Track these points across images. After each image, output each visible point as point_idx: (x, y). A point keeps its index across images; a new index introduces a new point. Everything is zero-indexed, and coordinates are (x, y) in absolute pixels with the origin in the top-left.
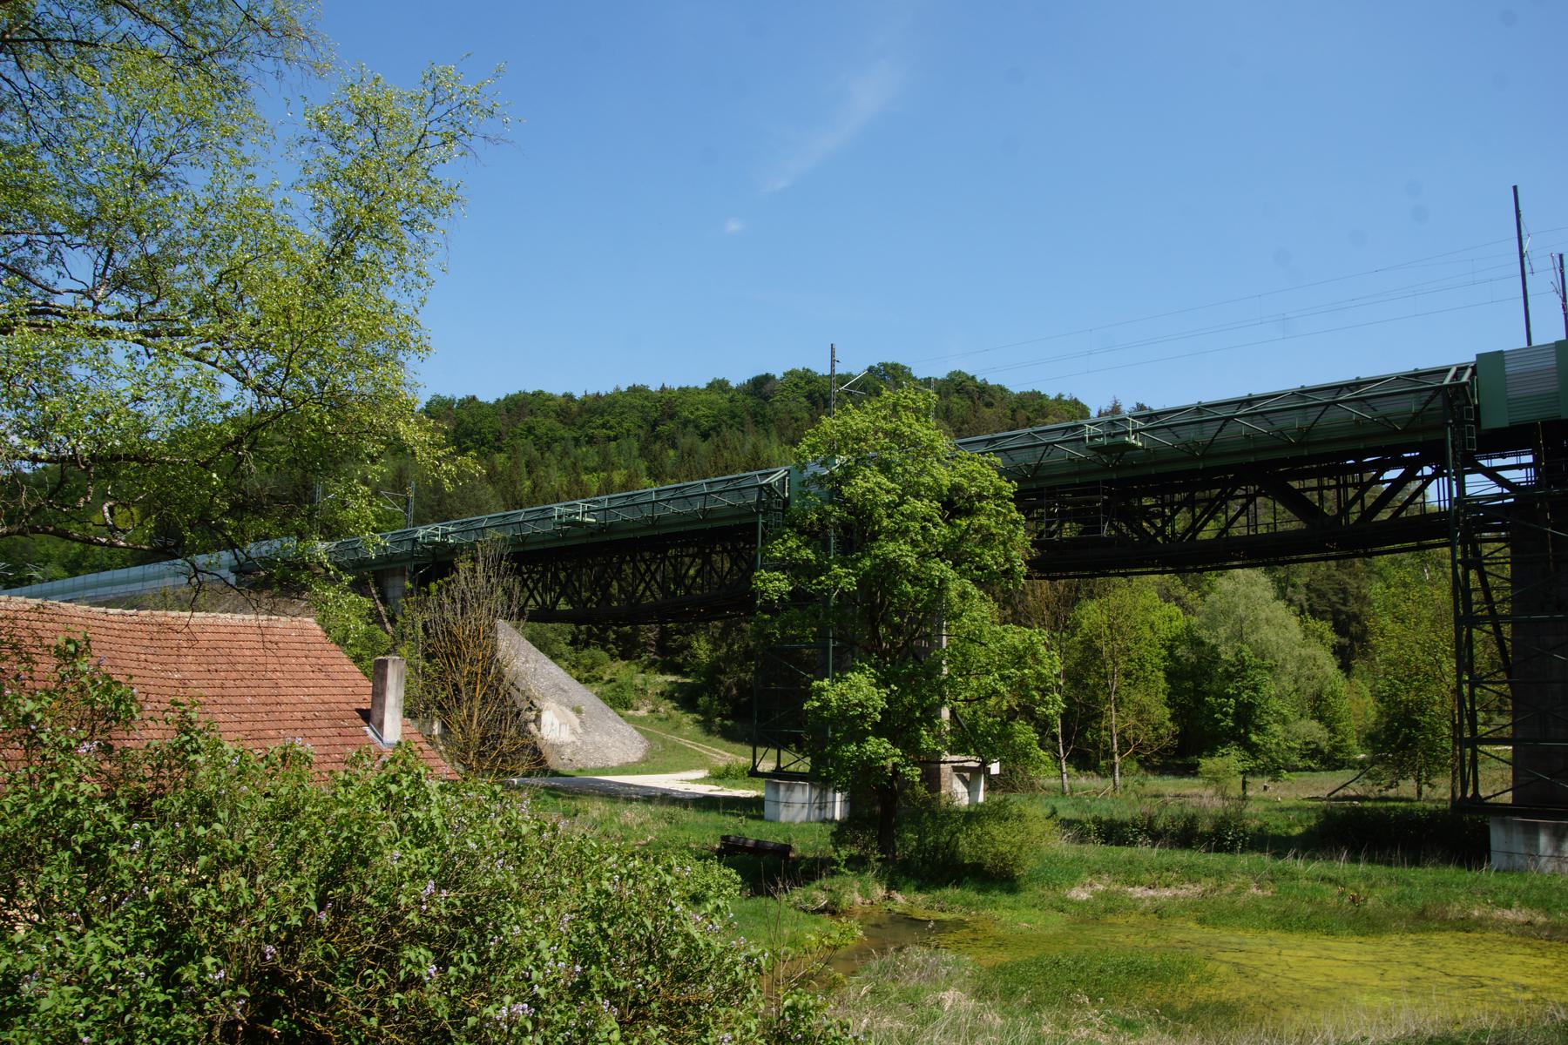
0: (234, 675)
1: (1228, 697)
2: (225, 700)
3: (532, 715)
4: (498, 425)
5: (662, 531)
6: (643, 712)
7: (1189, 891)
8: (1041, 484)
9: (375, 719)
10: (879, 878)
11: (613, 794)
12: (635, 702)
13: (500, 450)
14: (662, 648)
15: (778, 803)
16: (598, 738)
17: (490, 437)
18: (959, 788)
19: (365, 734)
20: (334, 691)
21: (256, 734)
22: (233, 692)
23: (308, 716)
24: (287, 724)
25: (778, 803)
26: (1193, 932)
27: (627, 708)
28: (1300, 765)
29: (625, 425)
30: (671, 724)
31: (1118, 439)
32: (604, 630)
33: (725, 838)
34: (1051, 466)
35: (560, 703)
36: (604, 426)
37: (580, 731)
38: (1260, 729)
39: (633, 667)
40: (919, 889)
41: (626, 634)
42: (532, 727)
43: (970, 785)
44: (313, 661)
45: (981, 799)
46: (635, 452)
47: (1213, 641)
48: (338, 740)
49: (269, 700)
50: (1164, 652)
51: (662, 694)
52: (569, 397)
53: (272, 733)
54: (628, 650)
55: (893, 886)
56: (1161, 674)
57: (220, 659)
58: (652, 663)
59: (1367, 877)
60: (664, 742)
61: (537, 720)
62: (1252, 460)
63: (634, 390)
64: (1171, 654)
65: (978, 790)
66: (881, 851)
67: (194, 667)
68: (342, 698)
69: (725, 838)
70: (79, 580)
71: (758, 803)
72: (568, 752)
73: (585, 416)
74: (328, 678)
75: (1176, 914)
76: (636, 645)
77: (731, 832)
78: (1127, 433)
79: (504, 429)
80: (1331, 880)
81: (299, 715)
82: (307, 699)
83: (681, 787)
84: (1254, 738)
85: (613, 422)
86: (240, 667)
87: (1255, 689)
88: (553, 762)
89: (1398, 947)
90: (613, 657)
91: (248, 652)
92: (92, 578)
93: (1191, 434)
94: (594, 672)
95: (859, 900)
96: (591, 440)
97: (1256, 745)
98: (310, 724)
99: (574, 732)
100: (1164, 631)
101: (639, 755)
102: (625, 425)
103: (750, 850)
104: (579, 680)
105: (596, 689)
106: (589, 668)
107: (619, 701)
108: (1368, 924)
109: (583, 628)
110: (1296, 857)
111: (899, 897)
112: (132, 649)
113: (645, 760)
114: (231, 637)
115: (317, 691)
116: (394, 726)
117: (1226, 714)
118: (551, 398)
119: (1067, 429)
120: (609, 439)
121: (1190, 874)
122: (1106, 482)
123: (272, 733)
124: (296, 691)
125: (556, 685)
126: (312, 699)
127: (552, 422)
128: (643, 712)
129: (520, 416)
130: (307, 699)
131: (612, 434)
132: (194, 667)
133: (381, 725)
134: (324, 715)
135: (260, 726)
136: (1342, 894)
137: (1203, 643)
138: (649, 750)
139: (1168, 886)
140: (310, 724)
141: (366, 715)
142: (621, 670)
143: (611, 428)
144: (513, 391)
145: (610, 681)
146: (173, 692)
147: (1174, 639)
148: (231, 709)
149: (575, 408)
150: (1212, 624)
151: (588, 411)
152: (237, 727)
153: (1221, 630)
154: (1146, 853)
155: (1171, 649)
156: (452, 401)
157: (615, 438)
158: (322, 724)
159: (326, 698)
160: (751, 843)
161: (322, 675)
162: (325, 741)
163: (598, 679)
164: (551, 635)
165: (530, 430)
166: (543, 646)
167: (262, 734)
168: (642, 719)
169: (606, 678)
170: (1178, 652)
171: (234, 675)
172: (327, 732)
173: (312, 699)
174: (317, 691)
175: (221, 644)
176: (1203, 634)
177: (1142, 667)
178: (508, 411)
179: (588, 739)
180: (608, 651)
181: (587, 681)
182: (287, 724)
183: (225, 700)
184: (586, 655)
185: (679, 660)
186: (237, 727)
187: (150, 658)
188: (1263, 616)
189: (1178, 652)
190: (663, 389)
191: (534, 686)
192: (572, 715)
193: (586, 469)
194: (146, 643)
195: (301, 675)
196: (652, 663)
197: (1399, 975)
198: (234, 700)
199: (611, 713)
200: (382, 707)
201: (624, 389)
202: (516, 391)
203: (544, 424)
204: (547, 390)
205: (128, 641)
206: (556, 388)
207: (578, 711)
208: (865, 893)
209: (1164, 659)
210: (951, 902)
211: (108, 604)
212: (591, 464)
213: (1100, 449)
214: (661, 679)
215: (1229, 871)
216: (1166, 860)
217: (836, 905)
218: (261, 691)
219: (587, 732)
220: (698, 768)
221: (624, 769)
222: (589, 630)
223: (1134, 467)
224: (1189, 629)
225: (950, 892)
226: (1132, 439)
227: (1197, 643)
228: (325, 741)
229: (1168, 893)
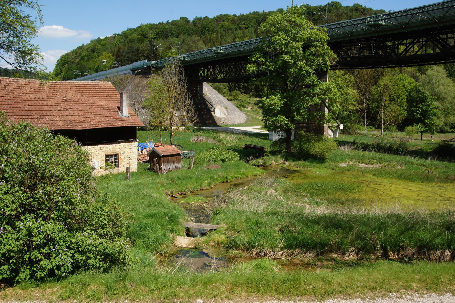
0: (82, 98)
1: (419, 108)
2: (78, 105)
3: (212, 110)
4: (214, 25)
5: (218, 59)
6: (249, 109)
7: (378, 166)
8: (354, 38)
9: (121, 109)
10: (282, 157)
11: (232, 132)
12: (247, 106)
13: (214, 32)
14: (256, 91)
15: (272, 135)
16: (232, 116)
17: (211, 29)
18: (330, 132)
19: (118, 113)
20: (112, 102)
21: (84, 114)
22: (80, 102)
23: (102, 109)
24: (95, 111)
25: (272, 135)
26: (370, 177)
27: (244, 108)
28: (449, 130)
29: (251, 24)
30: (256, 112)
31: (376, 22)
32: (239, 85)
33: (246, 144)
34: (357, 32)
35: (221, 106)
36: (244, 24)
37: (227, 114)
38: (429, 118)
39: (247, 96)
40: (294, 161)
41: (246, 86)
42: (212, 113)
43: (334, 132)
44: (107, 93)
45: (337, 136)
46: (253, 32)
47: (423, 91)
48: (109, 115)
49: (91, 105)
50: (407, 94)
51: (255, 104)
52: (235, 16)
53: (89, 113)
54: (246, 91)
55: (286, 159)
56: (405, 100)
57: (79, 94)
58: (253, 95)
59: (435, 165)
60: (252, 117)
61: (214, 111)
62: (441, 25)
63: (255, 13)
64: (409, 95)
65: (336, 133)
66: (286, 149)
67: (70, 96)
68: (114, 104)
69: (246, 144)
70: (98, 74)
71: (266, 135)
72: (223, 120)
73: (239, 21)
74: (111, 98)
75: (368, 172)
76: (249, 89)
77: (248, 143)
78: (380, 20)
79: (215, 26)
80: (424, 165)
81: (99, 109)
82: (103, 104)
83: (252, 130)
84: (426, 121)
85: (247, 23)
86: (84, 96)
87: (428, 106)
88: (218, 123)
89: (416, 186)
90: (242, 93)
91: (88, 92)
92: (101, 73)
93: (402, 20)
94: (236, 97)
95: (274, 163)
96: (240, 29)
97: (426, 123)
98: (102, 111)
99: (225, 114)
100: (408, 86)
101: (244, 121)
102: (251, 24)
103: (252, 148)
104: (228, 100)
105: (236, 102)
106: (234, 96)
107: (241, 106)
108: (427, 179)
109: (233, 84)
110: (415, 157)
111: (287, 163)
112: (53, 91)
113: (246, 123)
114: (84, 88)
115: (106, 102)
116: (126, 111)
117: (418, 113)
118: (230, 16)
119: (362, 19)
120: (246, 28)
121: (380, 160)
122: (375, 37)
123: (89, 113)
124: (100, 102)
125: (220, 101)
126: (104, 104)
127: (229, 23)
128: (249, 109)
129: (220, 22)
130: (103, 104)
131: (247, 26)
132: (70, 96)
133: (122, 111)
134: (107, 108)
135: (86, 112)
136: (426, 170)
137: (420, 91)
138: (248, 120)
139: (372, 164)
140: (102, 111)
141: (119, 108)
142: (244, 97)
143: (246, 25)
144: (219, 14)
145: (240, 100)
146: (63, 103)
147: (411, 90)
148: (78, 107)
149: (236, 18)
150: (423, 85)
151: (240, 19)
152: (79, 112)
153: (426, 87)
154: (373, 154)
155: (409, 93)
156: (201, 18)
157: (248, 28)
158: (106, 111)
159: (108, 104)
160: (252, 146)
161: (109, 98)
162: (105, 116)
163: (237, 99)
164: (222, 86)
165: (223, 26)
166: (219, 90)
167: (87, 114)
168: (248, 111)
169: (239, 99)
170: (412, 94)
171: (82, 98)
172: (106, 113)
173: (104, 104)
174: (106, 102)
175: (80, 90)
176: (420, 88)
177: (399, 98)
178: (217, 21)
179: (229, 116)
180: (240, 91)
181: (231, 100)
182: (95, 111)
183: (78, 105)
184: (234, 93)
185: (261, 94)
186: (79, 112)
187: (58, 94)
188: (441, 82)
189: (412, 94)
190: (264, 12)
191: (213, 101)
192: (224, 110)
193: (238, 37)
194: (58, 90)
195: (103, 98)
196: (253, 95)
197: (424, 195)
198: (80, 105)
199: (237, 109)
200: (122, 106)
201: (252, 12)
202: (219, 15)
203: (226, 24)
204: (228, 14)
205: (52, 90)
206: (231, 13)
207: (226, 108)
208: (276, 161)
209: (407, 96)
210: (299, 166)
211: (93, 81)
212: (240, 36)
213: (371, 26)
214: (255, 99)
215: (393, 161)
216: (374, 156)
217: (265, 164)
218: (89, 102)
219: (229, 114)
220: (258, 125)
221: (239, 125)
222: (235, 85)
223: (383, 32)
224: (416, 86)
225: (301, 162)
226: (381, 22)
227: (419, 91)
228: (105, 116)
229: (372, 166)
